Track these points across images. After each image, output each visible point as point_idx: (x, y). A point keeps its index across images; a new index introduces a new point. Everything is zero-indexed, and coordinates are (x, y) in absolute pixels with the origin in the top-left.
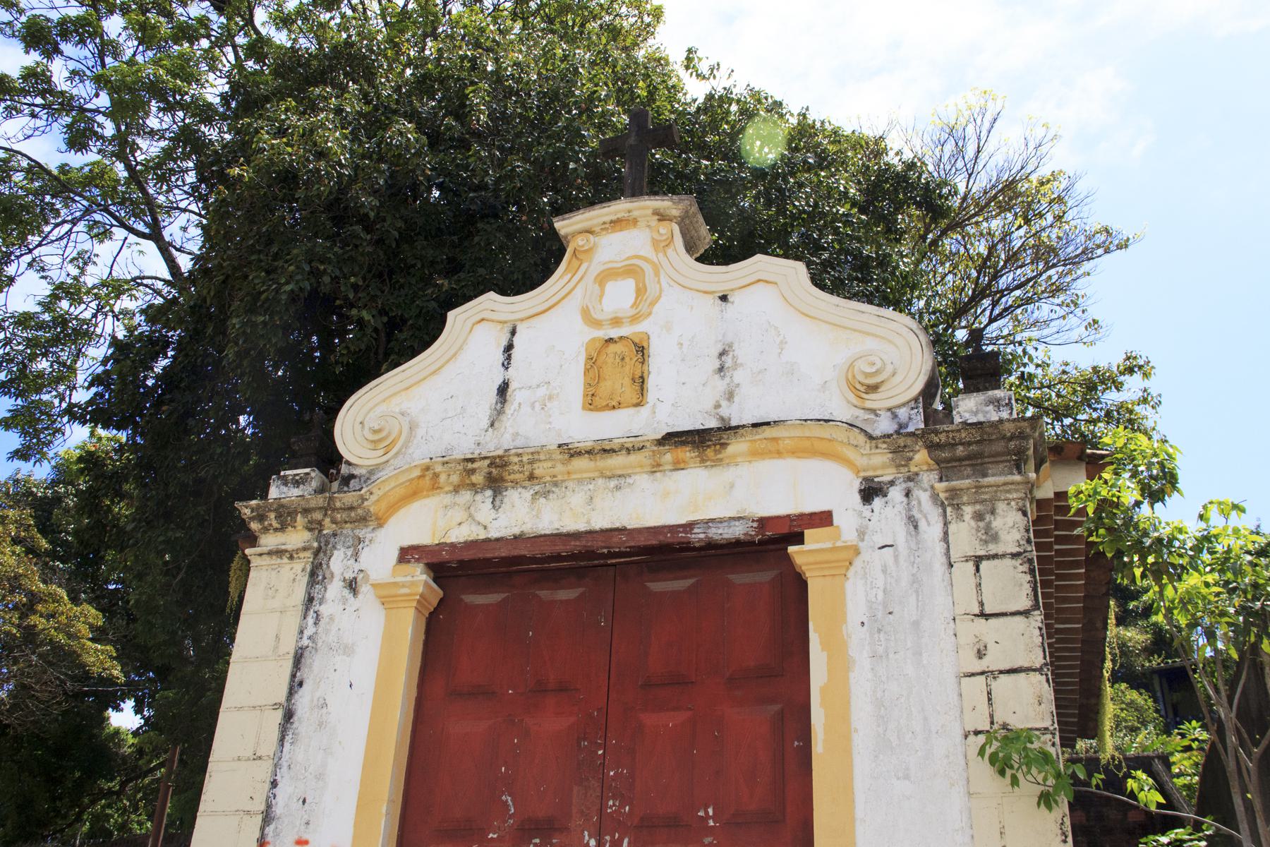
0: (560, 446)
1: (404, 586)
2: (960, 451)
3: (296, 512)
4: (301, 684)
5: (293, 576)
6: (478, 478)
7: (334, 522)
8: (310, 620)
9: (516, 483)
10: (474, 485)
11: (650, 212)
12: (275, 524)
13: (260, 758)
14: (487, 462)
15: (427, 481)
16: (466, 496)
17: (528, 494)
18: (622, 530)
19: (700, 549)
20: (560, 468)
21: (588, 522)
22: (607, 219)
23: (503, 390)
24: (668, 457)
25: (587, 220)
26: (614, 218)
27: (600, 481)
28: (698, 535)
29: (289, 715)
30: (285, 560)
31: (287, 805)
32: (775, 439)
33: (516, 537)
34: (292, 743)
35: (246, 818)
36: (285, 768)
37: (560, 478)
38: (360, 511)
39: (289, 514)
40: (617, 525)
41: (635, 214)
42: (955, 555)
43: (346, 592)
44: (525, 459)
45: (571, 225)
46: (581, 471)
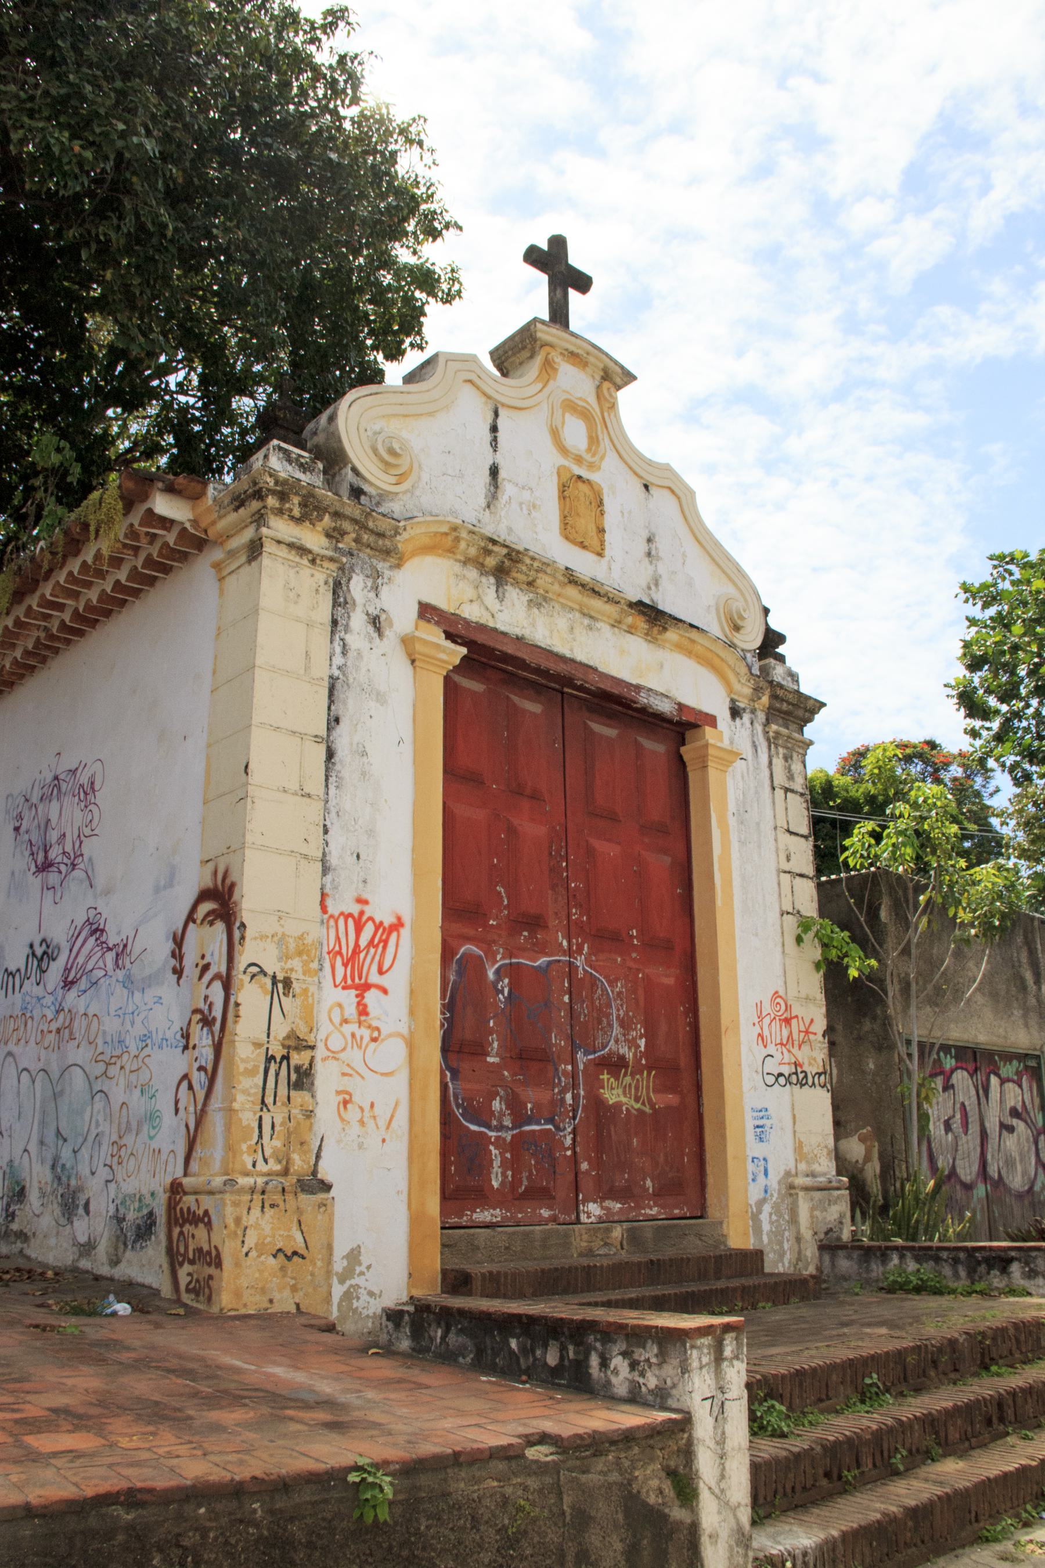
0: (567, 568)
1: (444, 651)
2: (785, 706)
3: (325, 510)
4: (337, 720)
5: (315, 586)
6: (491, 562)
7: (357, 540)
8: (338, 649)
9: (516, 583)
10: (483, 565)
11: (601, 366)
12: (296, 512)
13: (309, 796)
14: (505, 551)
15: (449, 541)
16: (473, 573)
17: (525, 598)
18: (595, 670)
19: (636, 710)
20: (556, 587)
21: (572, 650)
22: (572, 348)
23: (494, 471)
24: (630, 620)
25: (558, 338)
26: (576, 351)
27: (578, 615)
28: (643, 699)
29: (330, 754)
30: (305, 562)
31: (341, 857)
32: (693, 641)
33: (518, 638)
34: (337, 787)
35: (304, 862)
36: (333, 814)
37: (550, 595)
38: (387, 542)
39: (316, 508)
40: (591, 663)
41: (591, 359)
42: (776, 784)
43: (371, 629)
44: (536, 564)
45: (548, 333)
46: (568, 598)
